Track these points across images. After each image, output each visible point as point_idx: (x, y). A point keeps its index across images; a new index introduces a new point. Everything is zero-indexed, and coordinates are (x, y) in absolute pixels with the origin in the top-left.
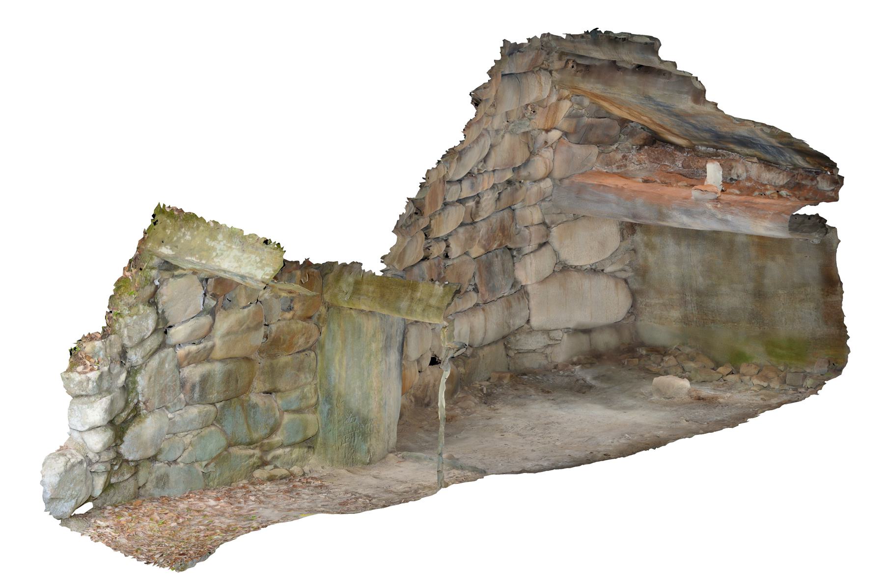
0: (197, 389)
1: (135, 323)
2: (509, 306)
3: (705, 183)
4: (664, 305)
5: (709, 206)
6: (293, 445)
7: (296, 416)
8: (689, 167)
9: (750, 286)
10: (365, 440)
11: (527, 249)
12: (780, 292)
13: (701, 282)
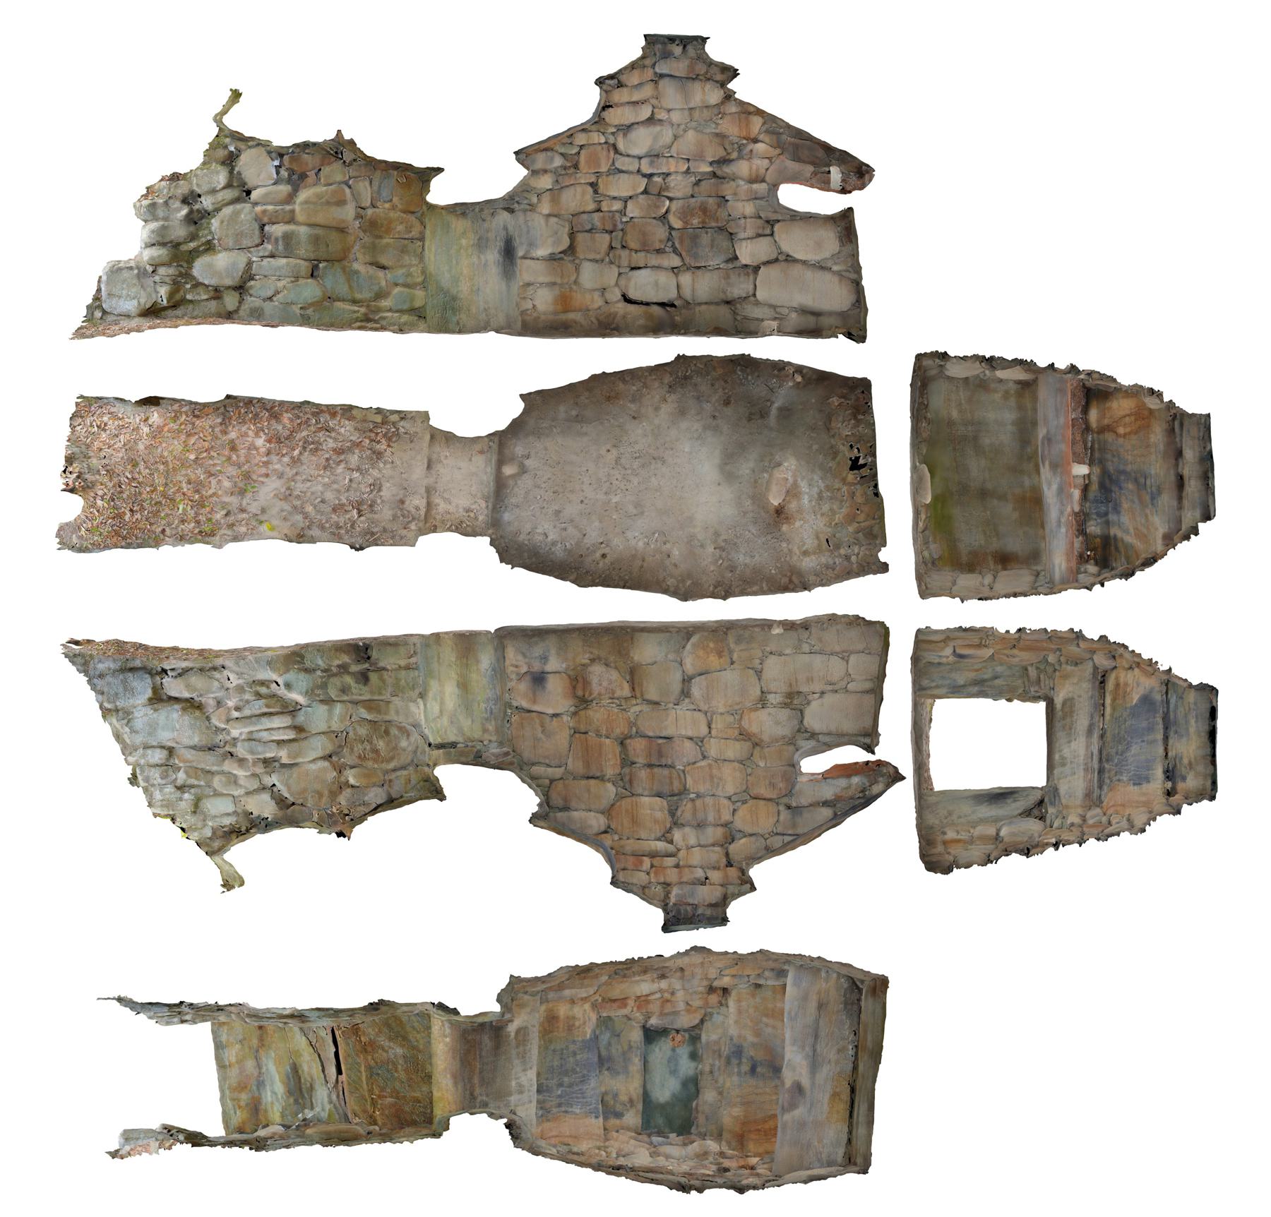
0: (280, 243)
1: (205, 175)
2: (727, 277)
4: (960, 404)
5: (1069, 509)
6: (401, 311)
7: (406, 290)
9: (989, 486)
10: (454, 314)
11: (742, 235)
13: (986, 441)
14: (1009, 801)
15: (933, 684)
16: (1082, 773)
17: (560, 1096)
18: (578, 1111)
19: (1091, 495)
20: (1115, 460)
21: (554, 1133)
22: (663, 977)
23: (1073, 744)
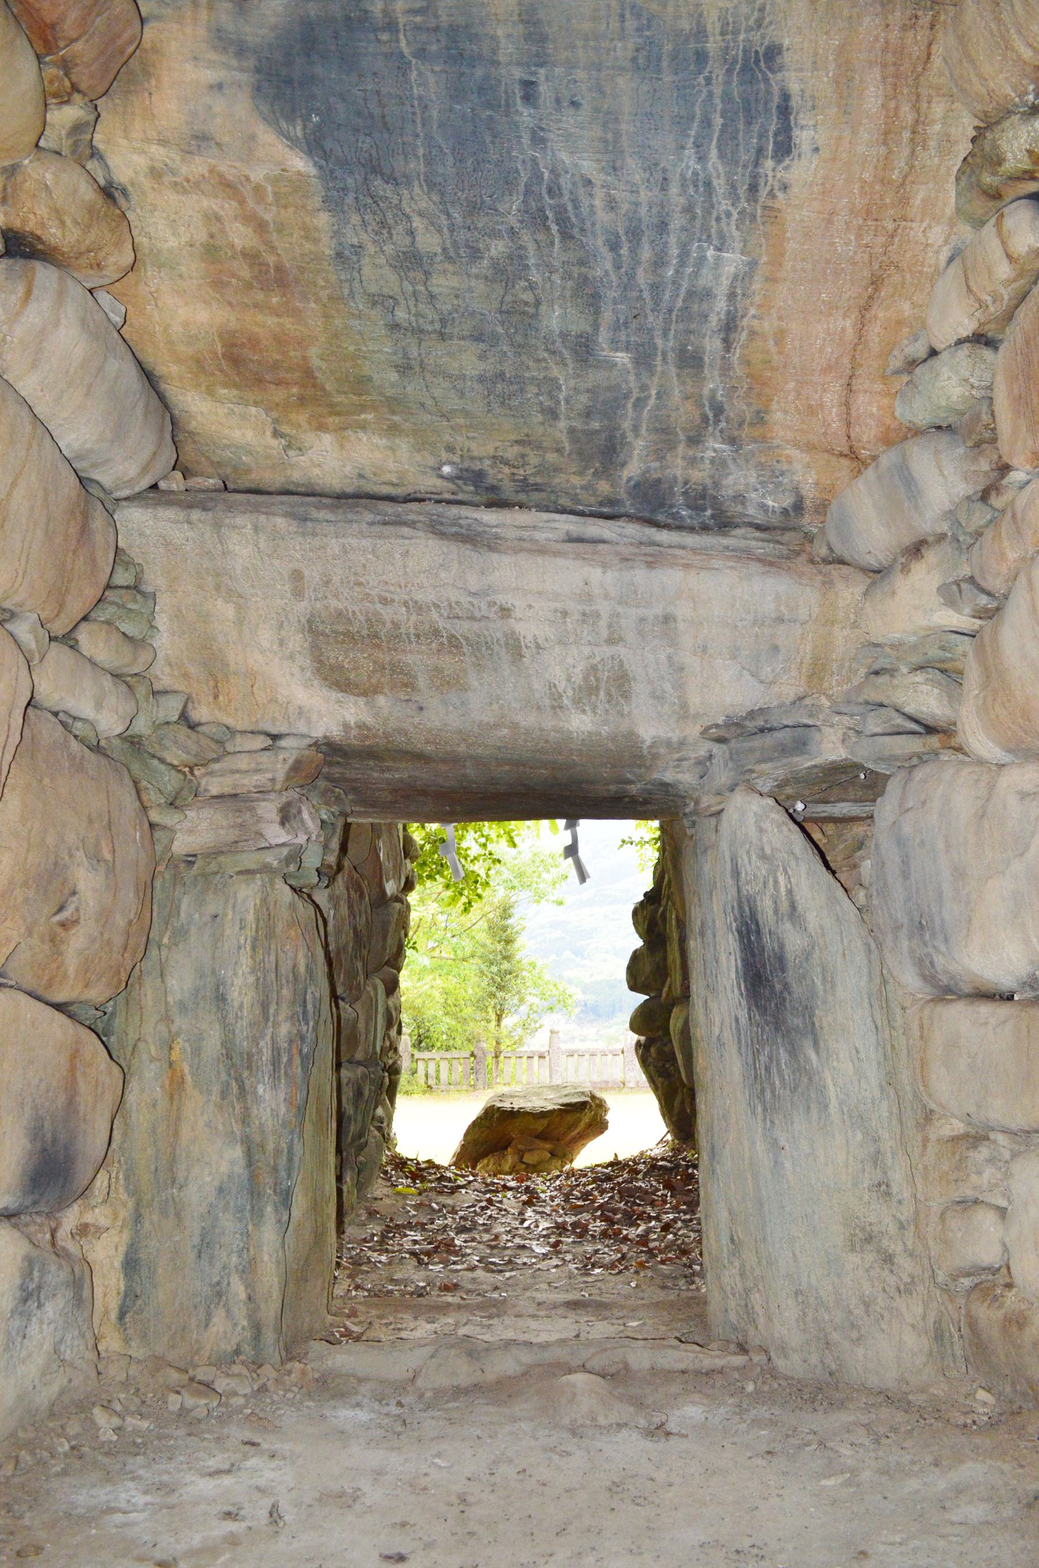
14: (794, 942)
15: (238, 1289)
16: (670, 578)
17: (644, 359)
18: (733, 261)
21: (831, 398)
23: (529, 628)
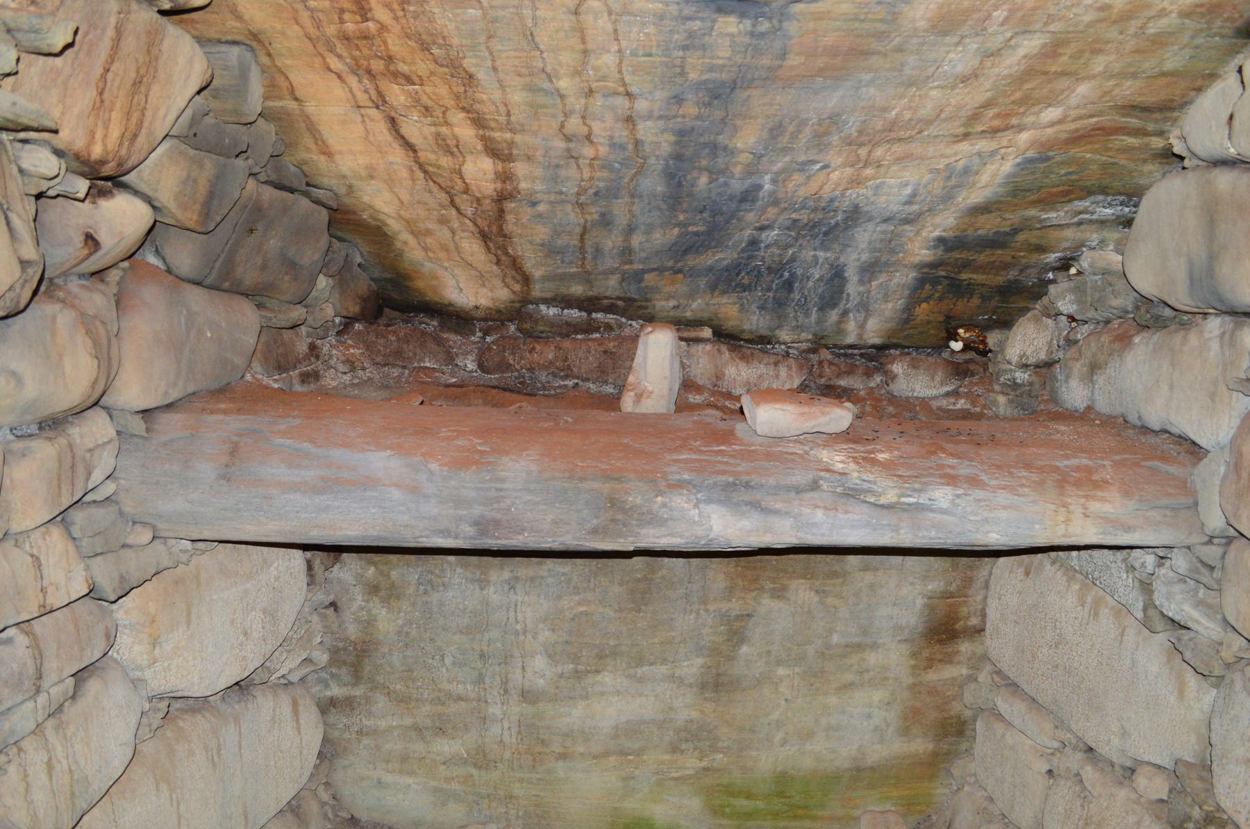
3: (628, 403)
5: (836, 458)
8: (504, 367)
12: (781, 671)
19: (755, 322)
20: (620, 210)
22: (596, 194)
